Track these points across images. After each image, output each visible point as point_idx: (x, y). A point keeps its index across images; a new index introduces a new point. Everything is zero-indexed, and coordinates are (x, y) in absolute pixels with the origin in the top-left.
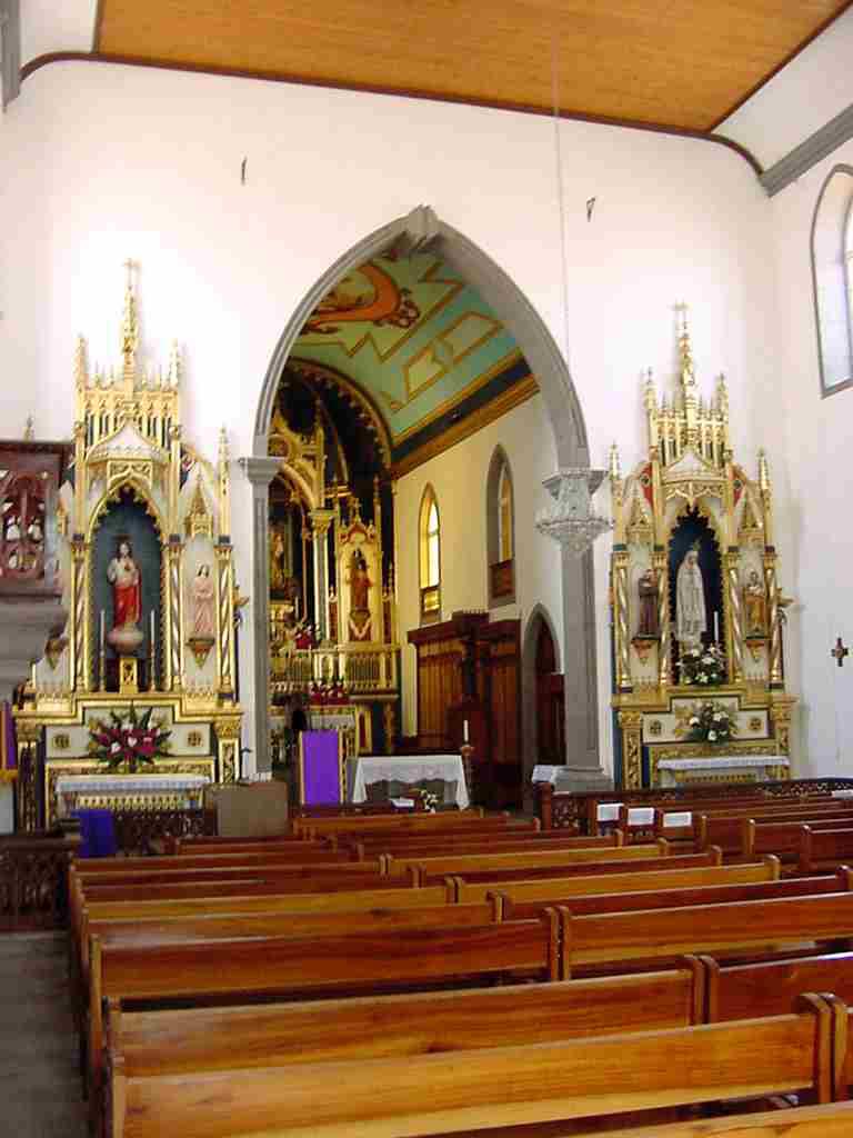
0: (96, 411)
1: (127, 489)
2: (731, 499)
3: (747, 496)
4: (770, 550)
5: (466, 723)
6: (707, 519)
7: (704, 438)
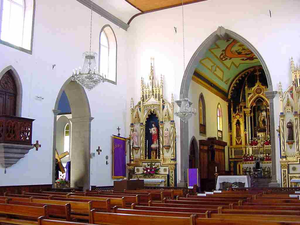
5: (216, 167)
6: (156, 114)
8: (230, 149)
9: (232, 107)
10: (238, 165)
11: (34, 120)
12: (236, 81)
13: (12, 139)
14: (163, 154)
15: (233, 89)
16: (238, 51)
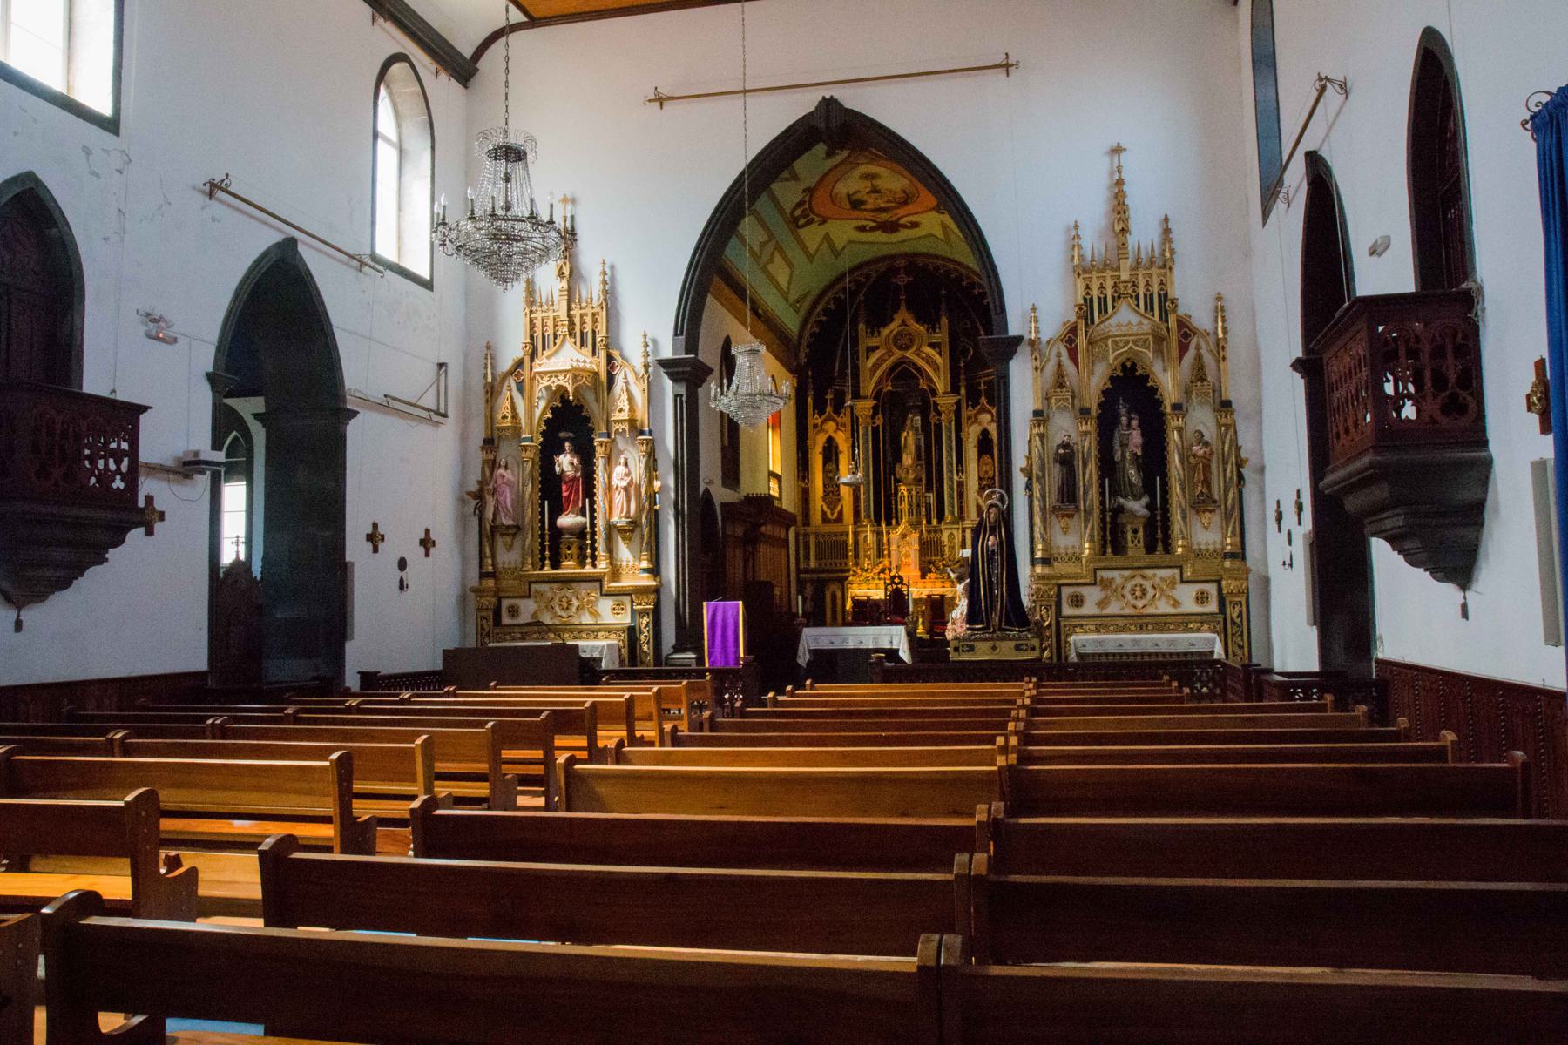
0: (1095, 293)
1: (1129, 364)
2: (1176, 353)
3: (1198, 348)
4: (1226, 404)
7: (1141, 290)
9: (811, 392)
11: (145, 409)
13: (56, 484)
14: (493, 557)
15: (817, 330)
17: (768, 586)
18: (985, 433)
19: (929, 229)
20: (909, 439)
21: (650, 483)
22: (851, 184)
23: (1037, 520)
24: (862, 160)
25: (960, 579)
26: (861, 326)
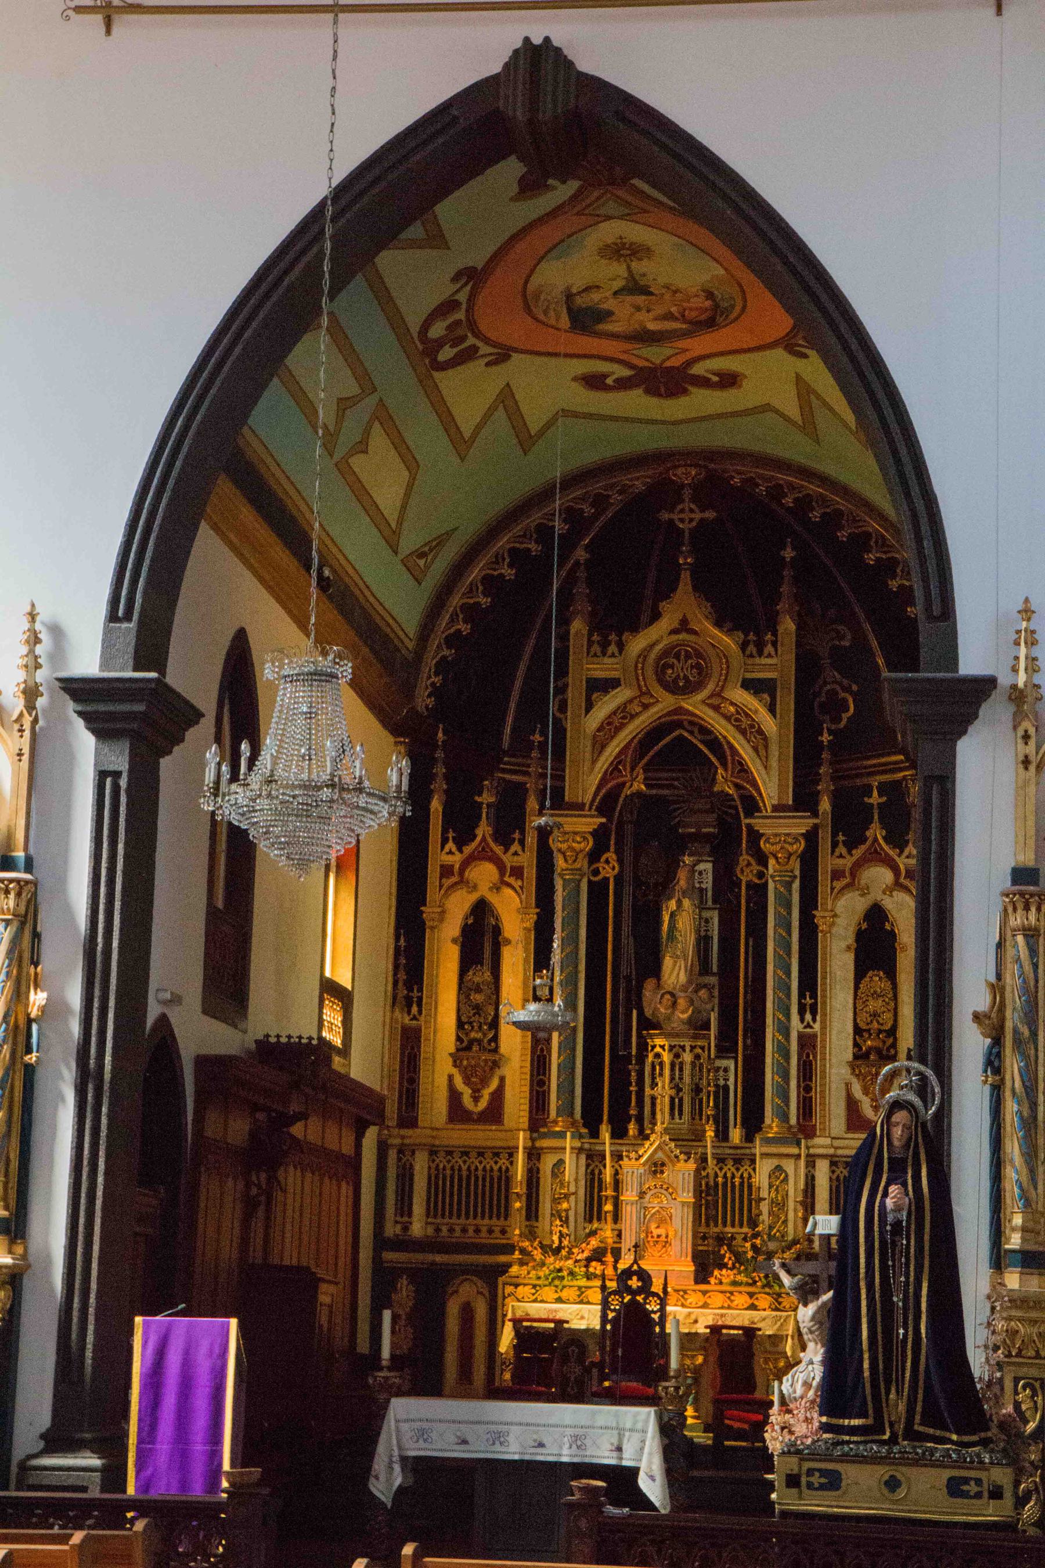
8: (392, 1154)
10: (453, 1309)
12: (498, 559)
16: (579, 301)
17: (303, 1282)
18: (876, 915)
19: (767, 394)
20: (682, 920)
21: (19, 995)
22: (579, 268)
23: (1013, 1149)
24: (611, 207)
25: (806, 1292)
26: (577, 626)
